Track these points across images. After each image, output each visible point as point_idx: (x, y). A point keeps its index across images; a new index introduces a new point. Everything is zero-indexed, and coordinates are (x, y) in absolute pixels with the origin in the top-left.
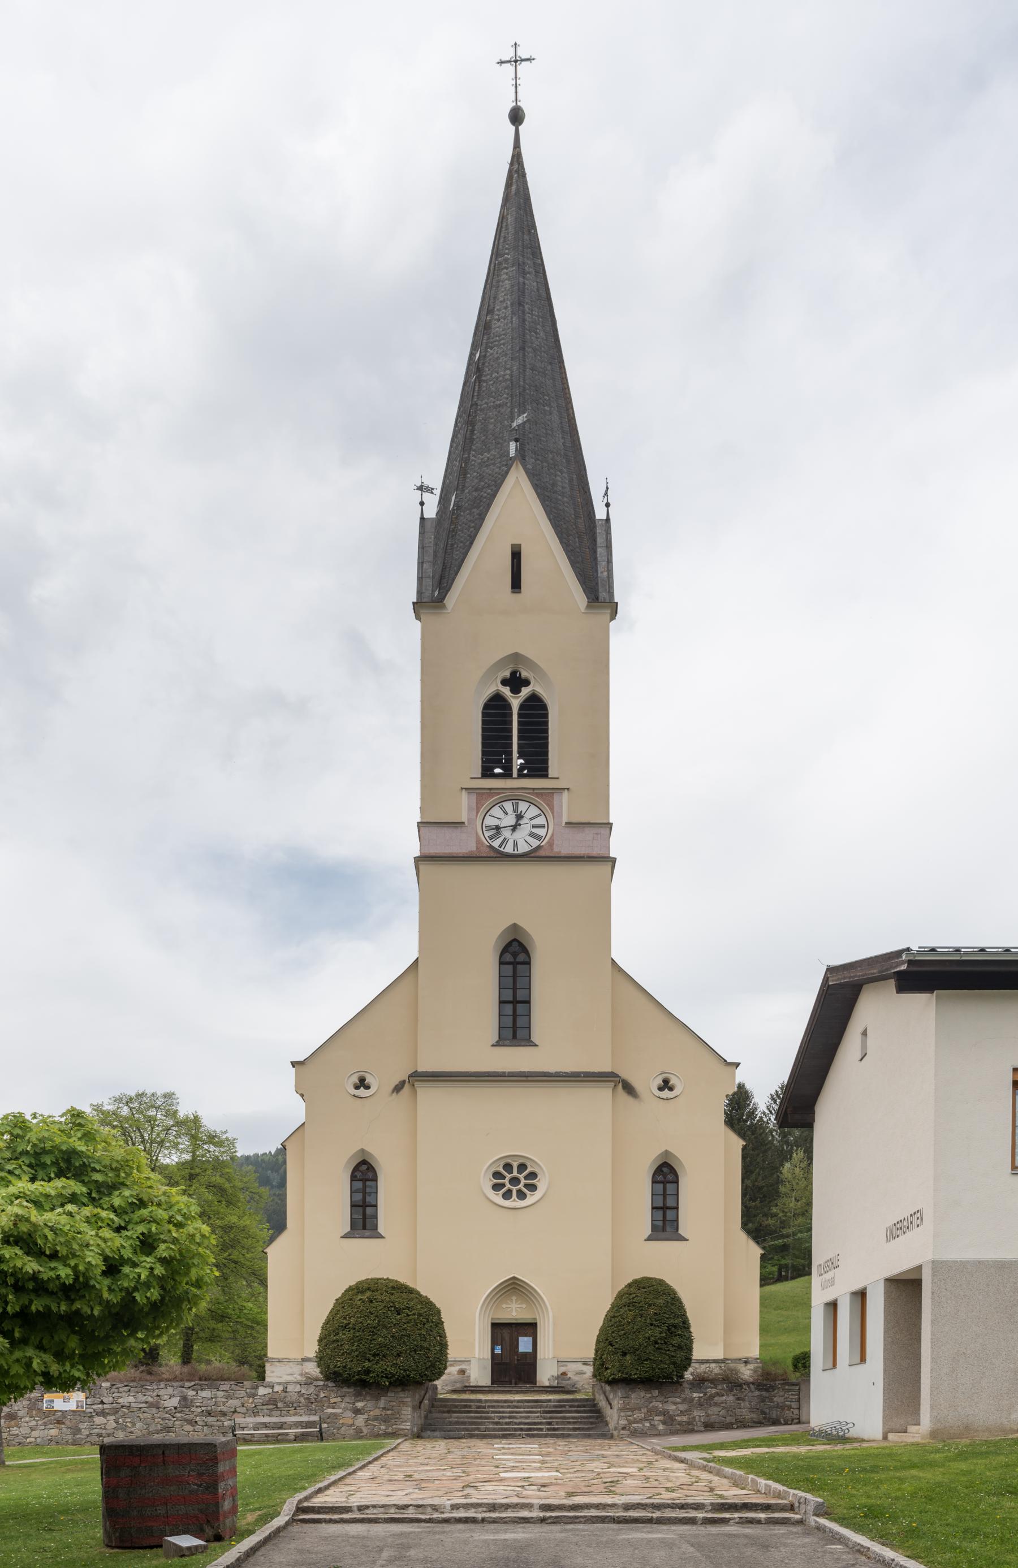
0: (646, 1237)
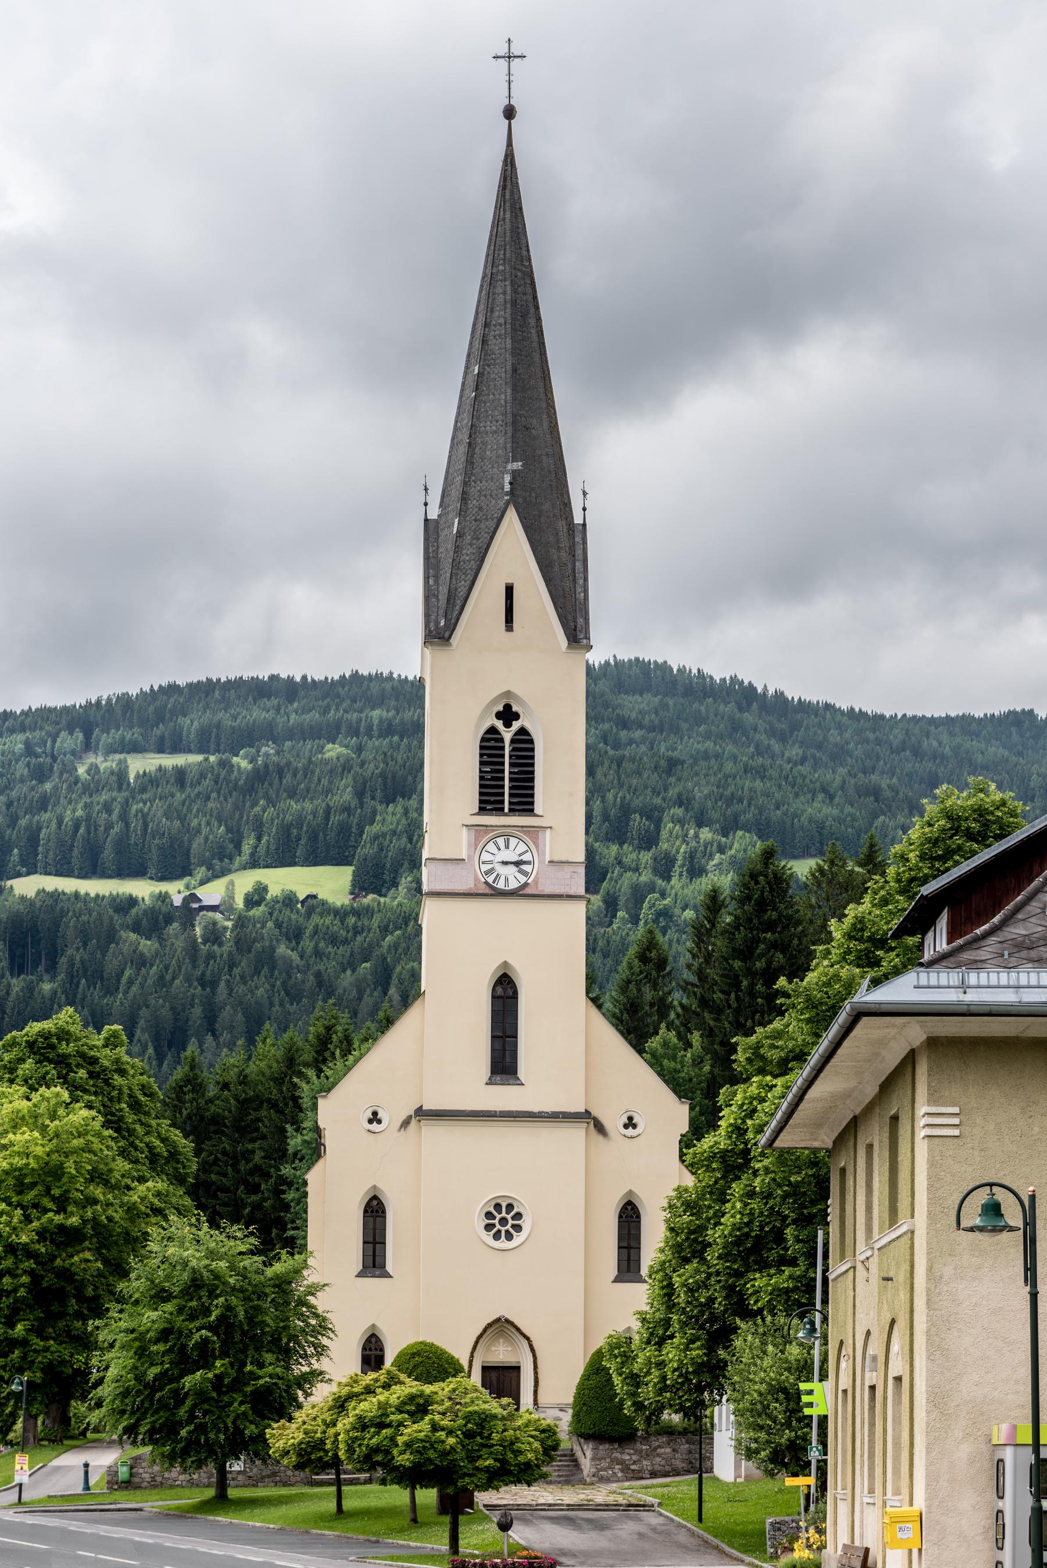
0: (612, 1279)
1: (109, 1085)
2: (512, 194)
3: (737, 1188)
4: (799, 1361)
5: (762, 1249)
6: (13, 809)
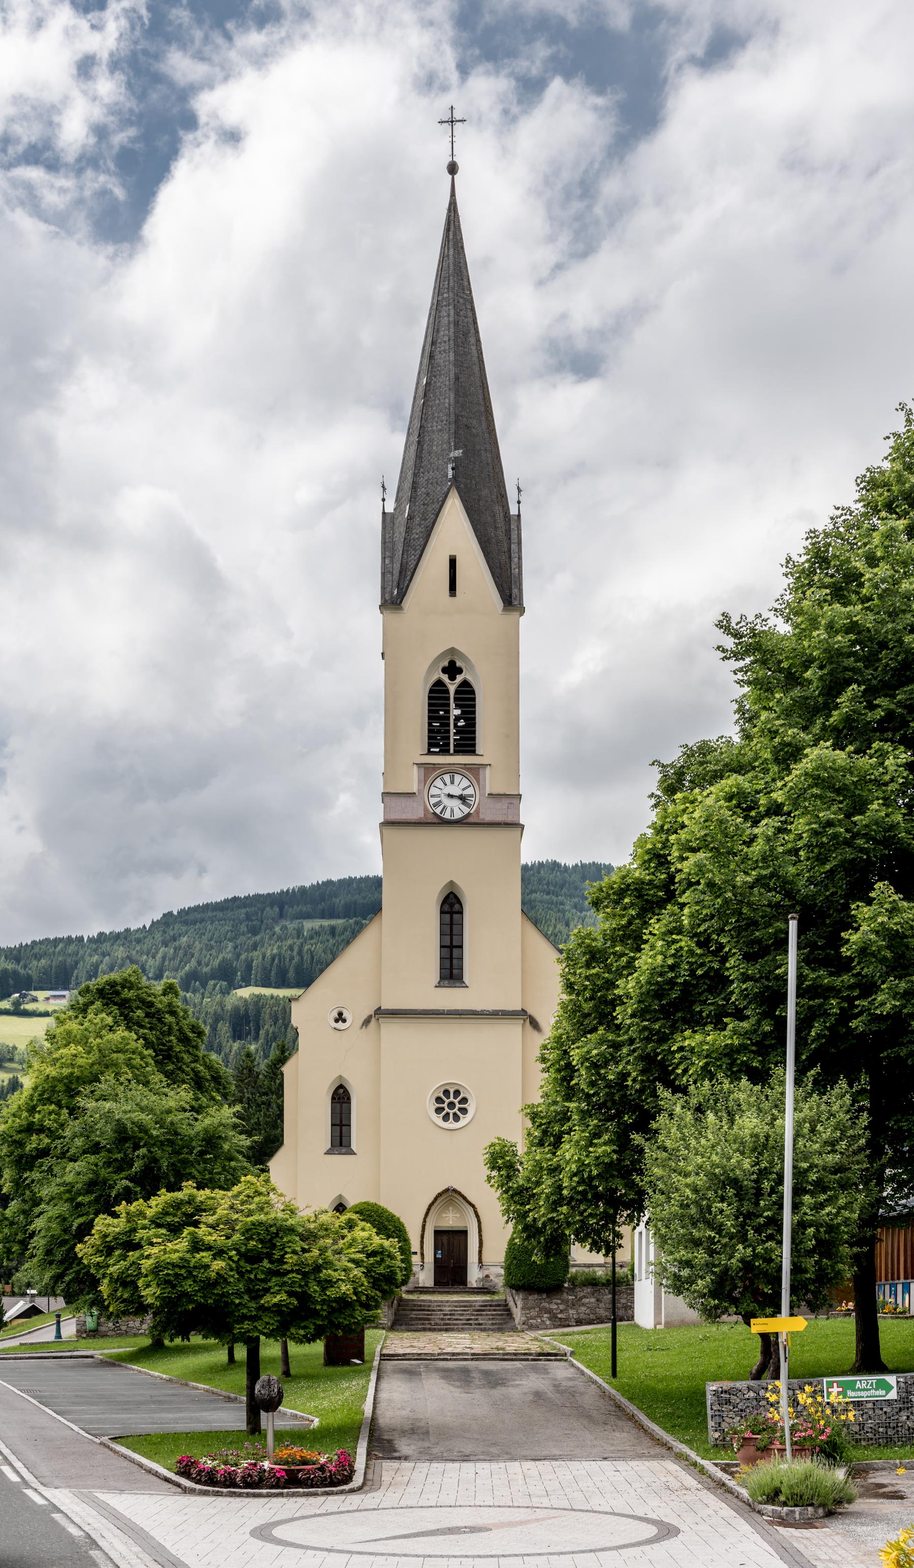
1: (162, 1023)
2: (455, 235)
3: (656, 926)
4: (756, 1136)
5: (694, 1002)
6: (238, 950)
